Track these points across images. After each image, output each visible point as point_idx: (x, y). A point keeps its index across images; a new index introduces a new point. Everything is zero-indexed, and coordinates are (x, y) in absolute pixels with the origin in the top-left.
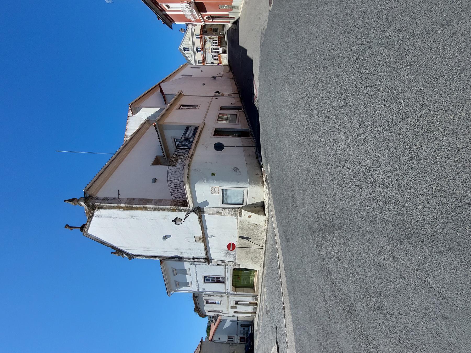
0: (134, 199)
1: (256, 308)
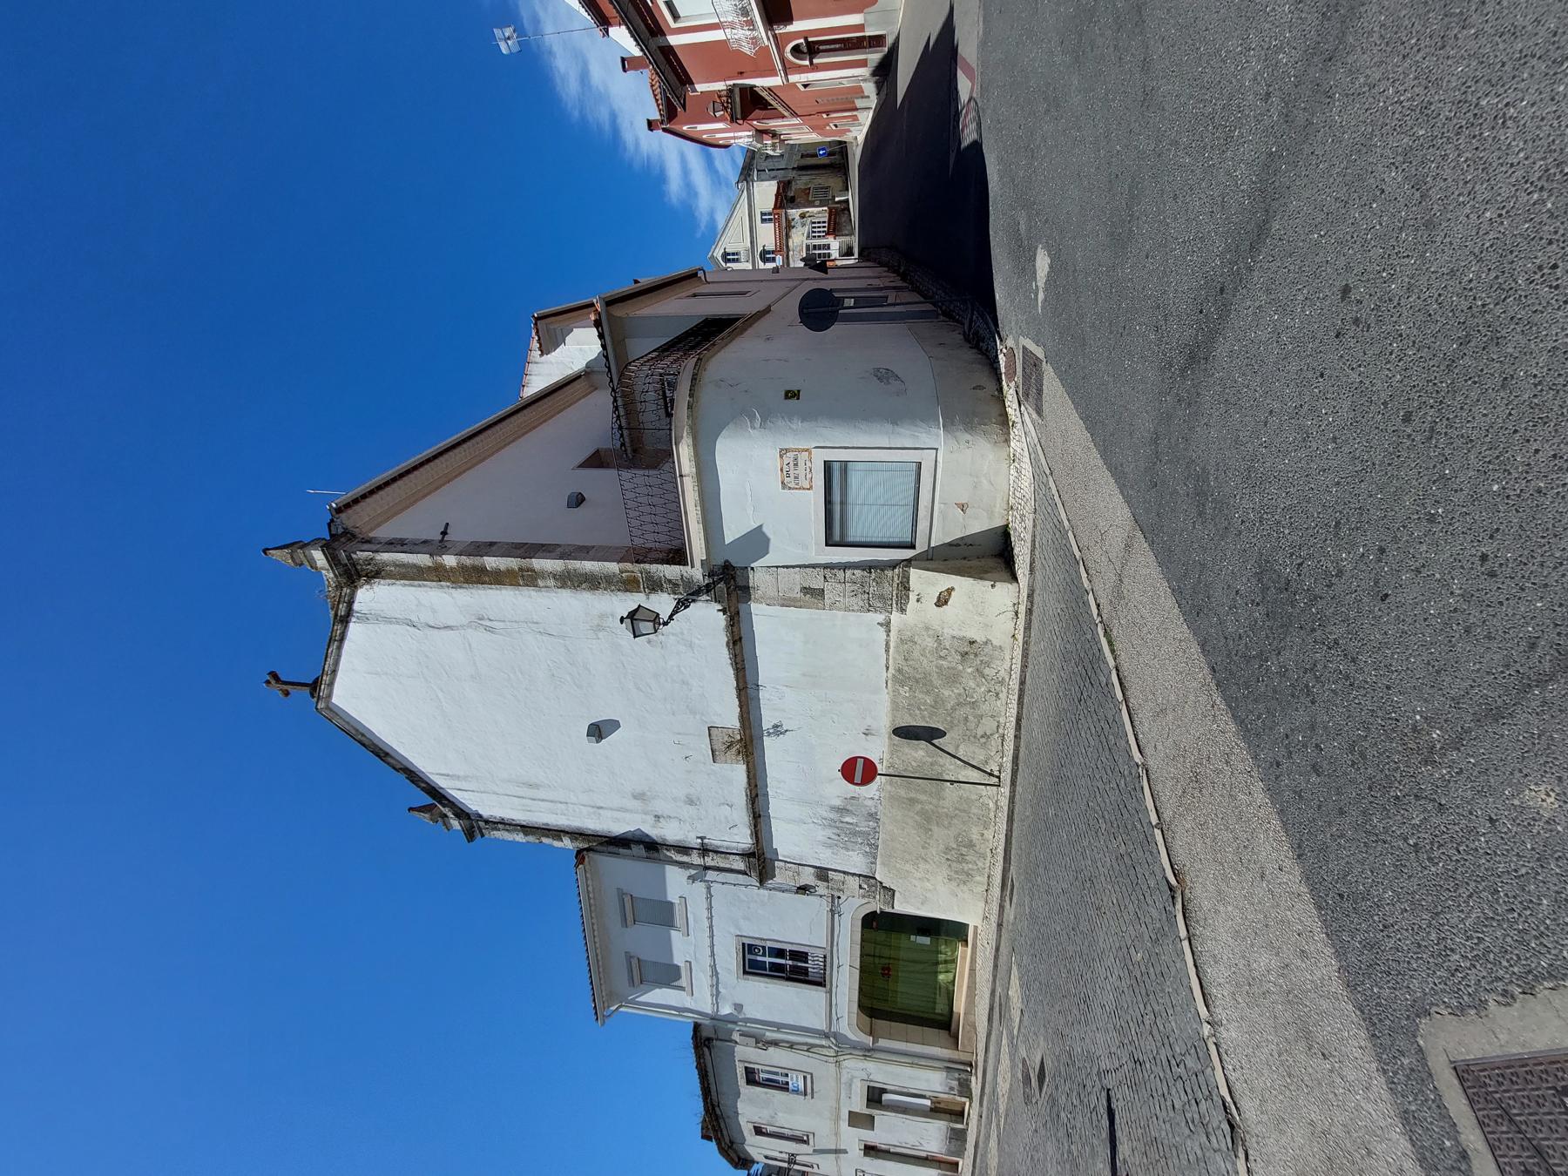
0: (492, 544)
1: (958, 1137)
